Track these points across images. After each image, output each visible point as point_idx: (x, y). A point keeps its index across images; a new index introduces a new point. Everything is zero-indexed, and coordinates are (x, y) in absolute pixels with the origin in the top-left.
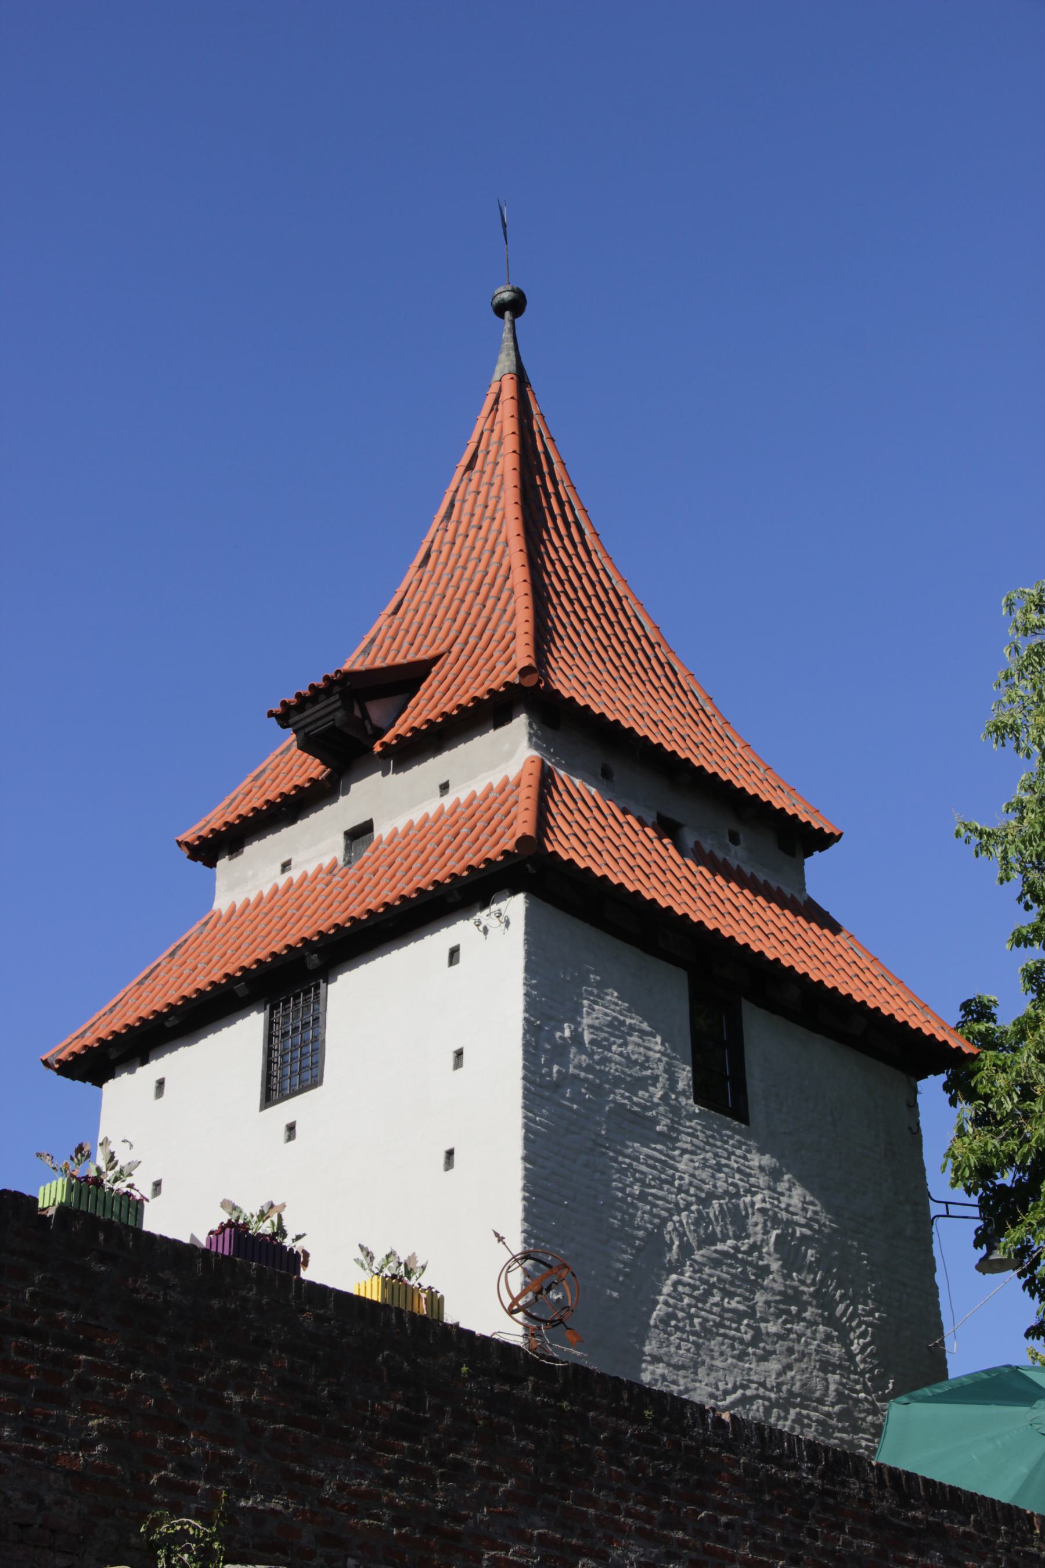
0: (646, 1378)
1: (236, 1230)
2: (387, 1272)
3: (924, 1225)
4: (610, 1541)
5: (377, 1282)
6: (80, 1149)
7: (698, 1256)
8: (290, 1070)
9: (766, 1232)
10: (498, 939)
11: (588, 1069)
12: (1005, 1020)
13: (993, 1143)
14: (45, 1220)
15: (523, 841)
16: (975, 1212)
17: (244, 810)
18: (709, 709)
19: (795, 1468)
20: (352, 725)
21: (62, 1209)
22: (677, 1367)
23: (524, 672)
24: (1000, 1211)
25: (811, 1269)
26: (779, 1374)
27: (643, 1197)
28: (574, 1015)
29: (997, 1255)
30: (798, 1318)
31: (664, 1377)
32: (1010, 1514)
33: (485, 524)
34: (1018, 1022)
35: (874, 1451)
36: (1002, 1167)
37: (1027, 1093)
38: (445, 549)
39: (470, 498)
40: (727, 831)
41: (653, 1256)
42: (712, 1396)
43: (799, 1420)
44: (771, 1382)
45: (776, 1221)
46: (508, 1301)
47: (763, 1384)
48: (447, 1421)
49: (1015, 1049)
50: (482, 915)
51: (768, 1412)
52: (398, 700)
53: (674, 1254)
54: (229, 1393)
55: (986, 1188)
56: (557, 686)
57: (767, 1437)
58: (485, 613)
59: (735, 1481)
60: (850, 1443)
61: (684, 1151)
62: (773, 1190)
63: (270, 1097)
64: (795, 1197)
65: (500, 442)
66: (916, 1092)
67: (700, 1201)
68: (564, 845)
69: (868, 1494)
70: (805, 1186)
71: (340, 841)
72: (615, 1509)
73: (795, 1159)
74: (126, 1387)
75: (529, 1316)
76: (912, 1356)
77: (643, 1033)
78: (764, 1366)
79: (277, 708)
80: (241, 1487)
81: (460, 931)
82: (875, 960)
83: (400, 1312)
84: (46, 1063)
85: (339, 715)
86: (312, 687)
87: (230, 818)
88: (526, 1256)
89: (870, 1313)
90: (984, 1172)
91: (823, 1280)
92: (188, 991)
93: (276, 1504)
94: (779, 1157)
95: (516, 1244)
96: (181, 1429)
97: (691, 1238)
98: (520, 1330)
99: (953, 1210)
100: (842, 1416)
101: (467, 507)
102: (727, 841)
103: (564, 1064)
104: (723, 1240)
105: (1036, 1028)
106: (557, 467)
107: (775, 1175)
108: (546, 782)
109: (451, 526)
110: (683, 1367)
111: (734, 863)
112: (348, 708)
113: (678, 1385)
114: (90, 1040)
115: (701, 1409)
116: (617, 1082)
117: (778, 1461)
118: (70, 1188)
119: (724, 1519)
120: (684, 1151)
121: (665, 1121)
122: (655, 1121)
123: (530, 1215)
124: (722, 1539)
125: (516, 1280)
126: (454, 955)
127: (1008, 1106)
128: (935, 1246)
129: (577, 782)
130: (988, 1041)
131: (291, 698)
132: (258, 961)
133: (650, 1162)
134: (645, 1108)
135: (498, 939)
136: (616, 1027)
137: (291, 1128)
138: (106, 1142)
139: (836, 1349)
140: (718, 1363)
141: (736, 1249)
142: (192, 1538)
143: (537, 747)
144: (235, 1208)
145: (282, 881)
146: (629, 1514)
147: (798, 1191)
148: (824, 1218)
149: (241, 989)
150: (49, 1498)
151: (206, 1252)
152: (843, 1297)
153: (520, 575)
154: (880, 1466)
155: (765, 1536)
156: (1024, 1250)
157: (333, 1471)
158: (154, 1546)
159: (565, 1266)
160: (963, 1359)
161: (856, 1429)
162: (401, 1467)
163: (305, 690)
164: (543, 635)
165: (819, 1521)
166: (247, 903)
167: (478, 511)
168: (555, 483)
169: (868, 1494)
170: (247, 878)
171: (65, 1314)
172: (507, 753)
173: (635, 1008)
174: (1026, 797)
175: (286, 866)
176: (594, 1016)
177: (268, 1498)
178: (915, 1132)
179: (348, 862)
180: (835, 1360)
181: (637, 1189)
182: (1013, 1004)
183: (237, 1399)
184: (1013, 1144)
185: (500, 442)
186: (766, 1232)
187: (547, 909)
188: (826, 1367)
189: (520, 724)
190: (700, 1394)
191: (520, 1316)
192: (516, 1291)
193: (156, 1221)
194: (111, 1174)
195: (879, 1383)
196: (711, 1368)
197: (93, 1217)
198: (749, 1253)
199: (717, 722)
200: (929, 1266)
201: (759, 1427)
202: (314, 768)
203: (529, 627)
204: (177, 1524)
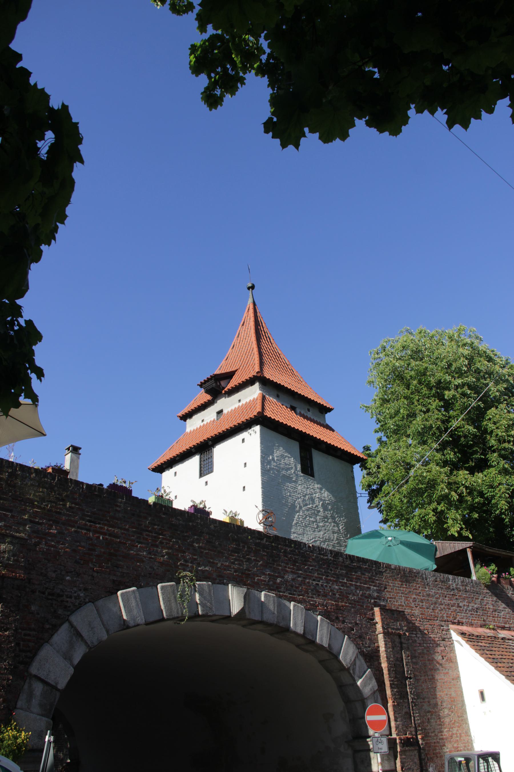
0: (292, 537)
1: (195, 507)
2: (230, 516)
3: (356, 498)
4: (284, 574)
5: (228, 518)
6: (157, 489)
7: (303, 509)
8: (206, 469)
9: (319, 502)
10: (254, 436)
11: (276, 466)
12: (373, 451)
13: (371, 479)
14: (150, 505)
15: (259, 413)
16: (367, 495)
17: (193, 408)
18: (301, 380)
19: (327, 556)
20: (217, 387)
21: (154, 503)
22: (299, 534)
23: (258, 373)
24: (373, 494)
25: (330, 511)
26: (323, 535)
27: (290, 496)
28: (272, 454)
29: (373, 505)
30: (327, 522)
31: (296, 537)
32: (376, 563)
33: (247, 338)
34: (376, 451)
35: (345, 551)
36: (373, 485)
37: (379, 467)
38: (238, 344)
39: (243, 332)
41: (293, 509)
42: (307, 541)
43: (328, 545)
44: (321, 537)
45: (321, 500)
46: (259, 521)
47: (319, 537)
48: (246, 549)
49: (375, 457)
50: (250, 431)
51: (320, 543)
52: (228, 380)
53: (298, 508)
54: (195, 544)
55: (370, 489)
56: (265, 376)
57: (320, 549)
58: (248, 359)
59: (313, 559)
60: (340, 549)
61: (299, 485)
62: (320, 493)
63: (201, 475)
64: (326, 494)
65: (250, 319)
66: (353, 468)
67: (303, 496)
68: (268, 413)
69: (344, 561)
70: (328, 491)
71: (215, 414)
72: (286, 567)
73: (326, 485)
74: (171, 543)
75: (264, 524)
76: (354, 529)
77: (289, 457)
78: (320, 533)
79: (200, 384)
80: (199, 565)
81: (244, 435)
82: (343, 438)
83: (234, 525)
84: (149, 469)
85: (214, 384)
86: (207, 378)
87: (189, 410)
88: (263, 511)
89: (344, 520)
90: (369, 486)
91: (333, 513)
92: (181, 451)
93: (207, 568)
94: (322, 484)
95: (261, 508)
96: (184, 552)
97: (302, 505)
98: (262, 528)
99: (362, 495)
100: (337, 543)
101: (243, 334)
103: (270, 465)
104: (309, 505)
105: (380, 452)
106: (263, 324)
107: (321, 489)
108: (264, 398)
109: (239, 339)
110: (301, 534)
111: (309, 416)
112: (216, 382)
113: (300, 539)
114: (159, 463)
115: (305, 544)
116: (283, 469)
117: (323, 554)
118: (156, 498)
119: (311, 568)
120: (299, 485)
121: (295, 478)
122: (292, 478)
123: (264, 501)
124: (310, 572)
125: (261, 516)
126: (243, 440)
127: (374, 470)
128: (358, 504)
129: (271, 398)
130: (369, 456)
131: (203, 381)
132: (197, 444)
134: (290, 475)
135: (254, 436)
136: (282, 456)
137: (206, 483)
138: (163, 487)
139: (336, 529)
140: (309, 533)
141: (312, 507)
142: (188, 576)
143: (261, 390)
144: (194, 502)
145: (202, 424)
146: (289, 568)
147: (326, 493)
148: (332, 499)
149: (193, 450)
150: (155, 568)
151: (188, 512)
152: (337, 517)
153: (256, 350)
154: (346, 554)
155: (320, 571)
156: (378, 503)
157: (220, 561)
158: (180, 578)
159: (272, 513)
160: (365, 529)
161: (341, 546)
162: (235, 560)
163: (206, 379)
164: (262, 364)
165: (333, 567)
166: (194, 430)
167: (245, 335)
168: (263, 328)
169: (344, 561)
170: (194, 424)
171: (156, 527)
172: (254, 392)
173: (287, 451)
174: (376, 398)
175: (203, 421)
176: (278, 453)
177: (205, 567)
178: (353, 478)
179: (217, 419)
180: (336, 531)
181: (288, 494)
182: (375, 447)
183: (197, 545)
184: (376, 479)
185: (250, 319)
186: (319, 502)
187: (265, 429)
188: (334, 533)
189: (257, 385)
190: (305, 540)
191: (262, 524)
192: (261, 519)
193: (176, 505)
194: (165, 495)
195: (346, 535)
196: (307, 534)
197: (161, 505)
198: (315, 507)
199: (304, 383)
200: (357, 508)
201: (319, 547)
202: (209, 397)
203: (258, 362)
204: (185, 573)
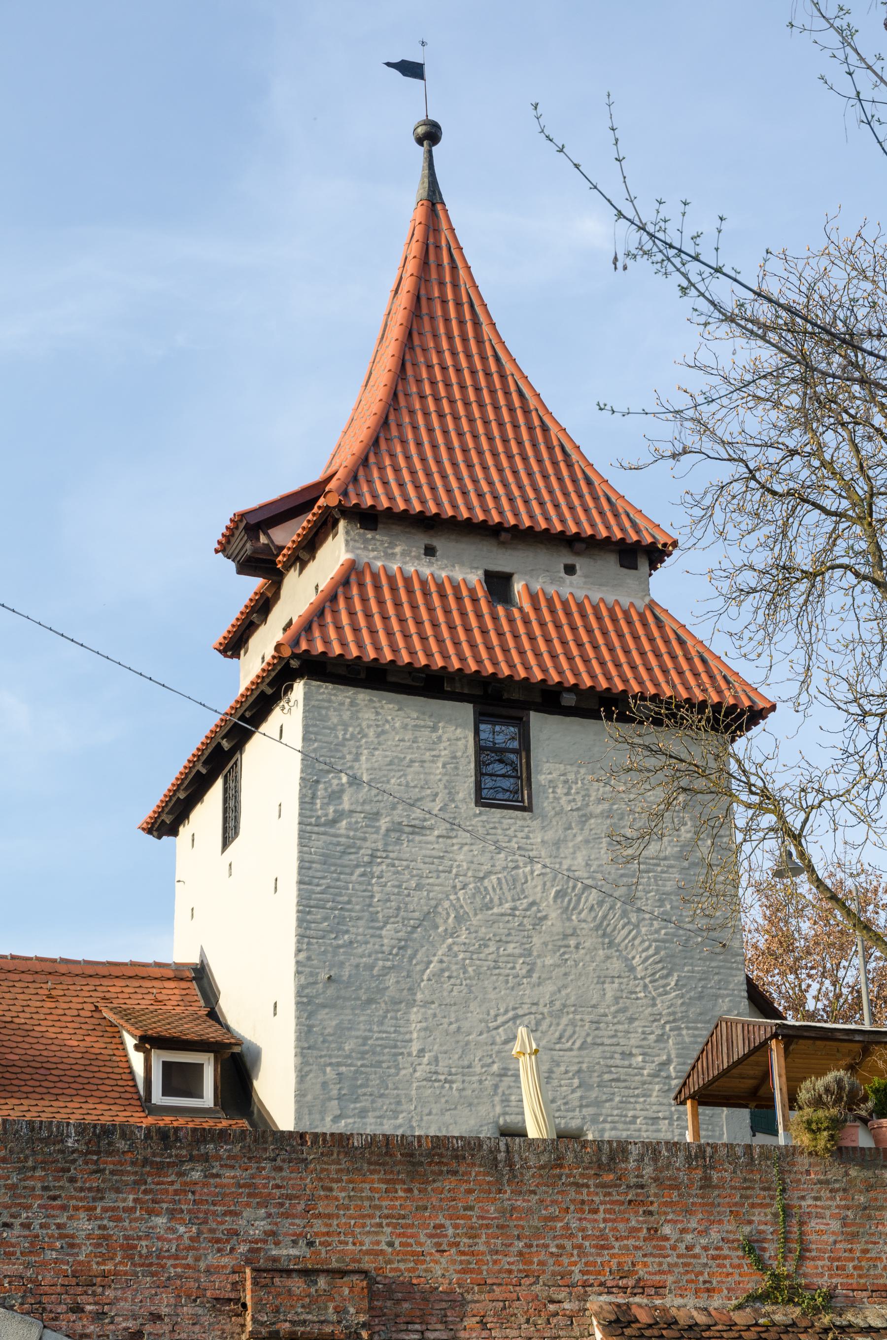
40: (562, 566)
102: (563, 574)
133: (427, 860)
202: (254, 584)
